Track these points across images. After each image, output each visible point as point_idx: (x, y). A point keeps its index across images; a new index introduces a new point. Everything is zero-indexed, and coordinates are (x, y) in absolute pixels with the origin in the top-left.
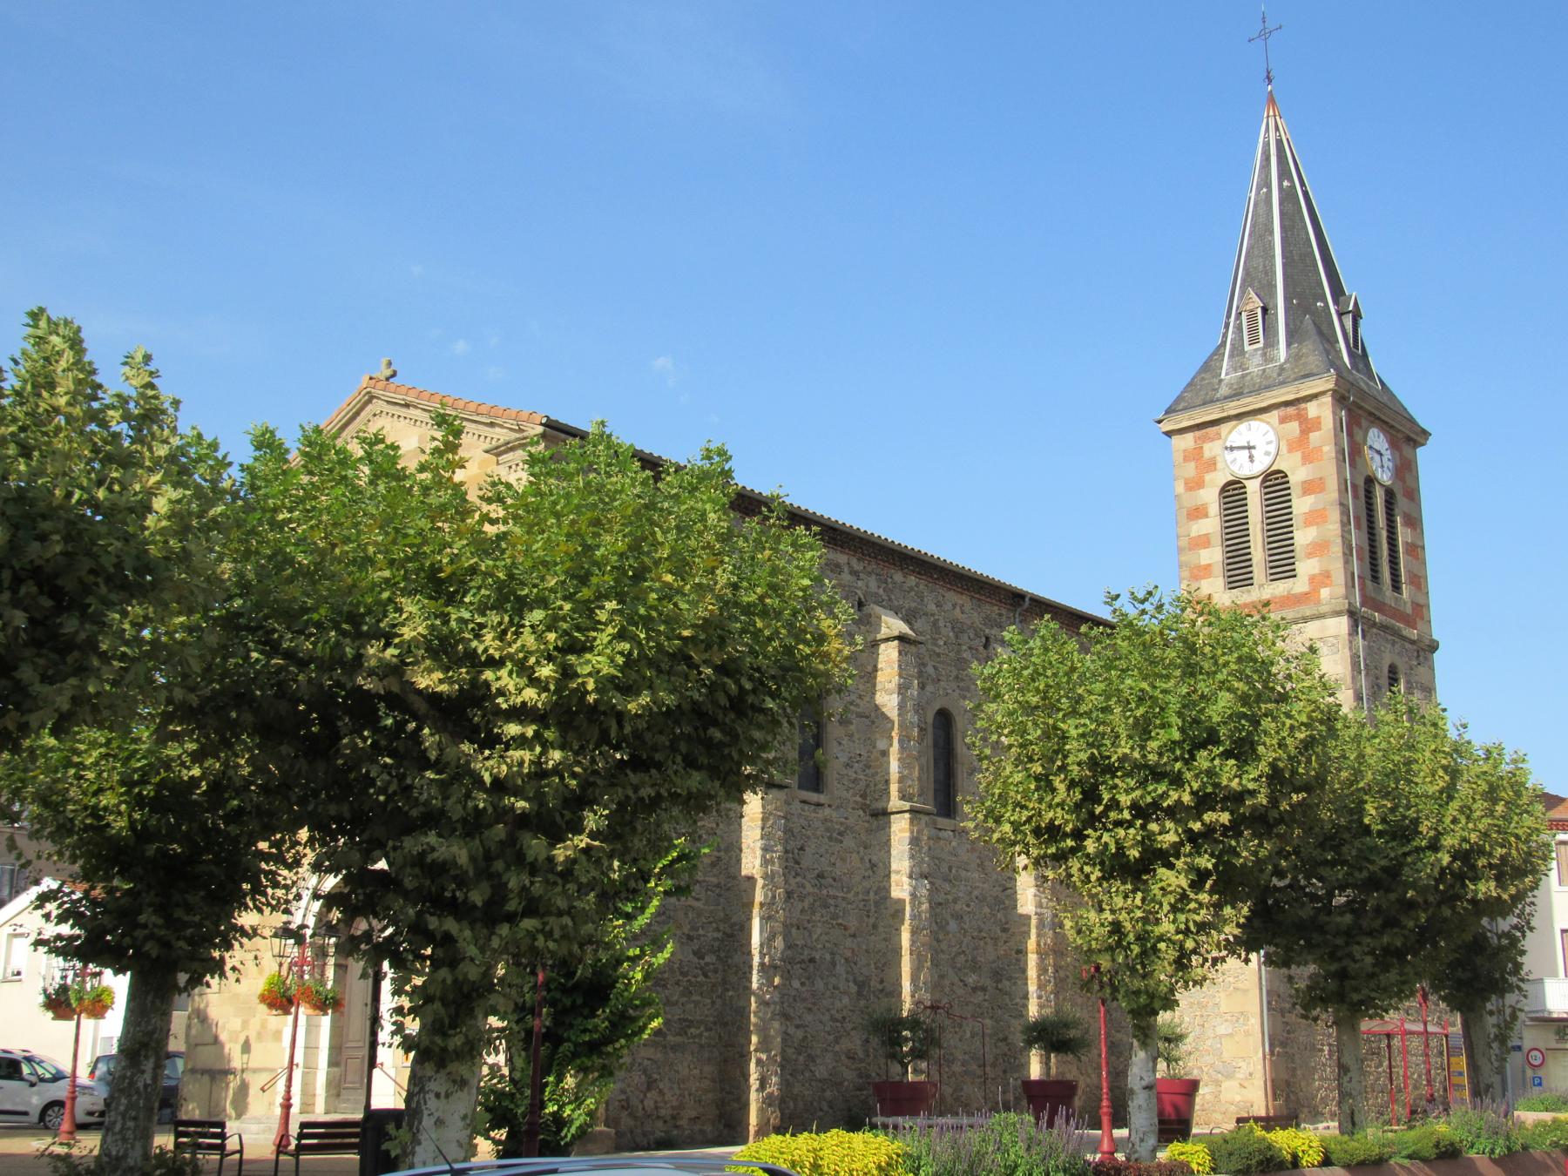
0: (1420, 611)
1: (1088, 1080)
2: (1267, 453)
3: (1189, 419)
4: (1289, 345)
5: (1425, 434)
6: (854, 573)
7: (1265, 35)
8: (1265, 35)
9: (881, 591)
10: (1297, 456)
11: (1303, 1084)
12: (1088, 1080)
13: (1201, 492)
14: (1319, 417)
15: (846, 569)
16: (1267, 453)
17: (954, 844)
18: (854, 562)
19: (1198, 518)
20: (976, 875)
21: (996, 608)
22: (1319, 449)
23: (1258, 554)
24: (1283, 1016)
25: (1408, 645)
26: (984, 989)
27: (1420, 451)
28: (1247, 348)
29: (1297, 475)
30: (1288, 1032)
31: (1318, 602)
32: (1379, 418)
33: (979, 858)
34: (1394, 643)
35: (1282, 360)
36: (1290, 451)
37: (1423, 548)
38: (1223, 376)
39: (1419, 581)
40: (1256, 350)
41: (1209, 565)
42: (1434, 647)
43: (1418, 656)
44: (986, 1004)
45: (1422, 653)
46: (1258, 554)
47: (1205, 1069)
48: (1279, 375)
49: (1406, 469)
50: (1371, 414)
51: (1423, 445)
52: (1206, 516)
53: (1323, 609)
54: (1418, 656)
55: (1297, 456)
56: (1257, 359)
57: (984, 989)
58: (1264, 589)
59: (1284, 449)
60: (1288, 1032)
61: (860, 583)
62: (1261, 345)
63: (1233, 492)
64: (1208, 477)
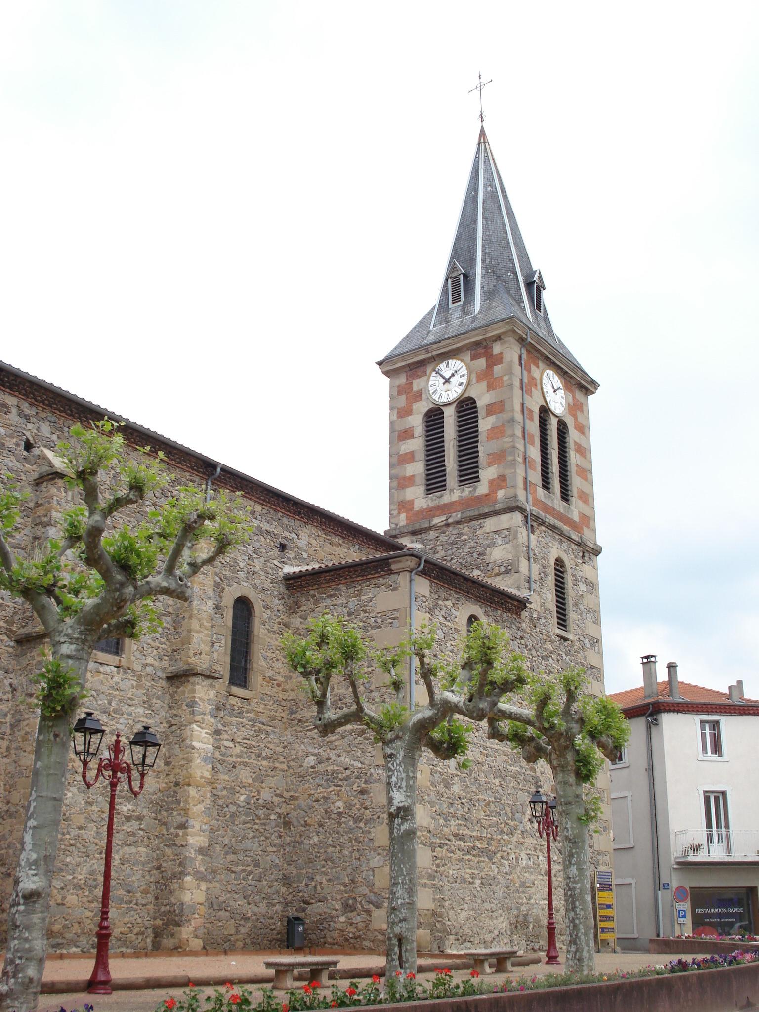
0: (588, 520)
1: (256, 909)
2: (461, 384)
3: (403, 361)
4: (483, 301)
5: (595, 384)
6: (21, 414)
7: (480, 87)
8: (480, 87)
9: (54, 437)
10: (484, 384)
11: (451, 913)
12: (256, 909)
13: (410, 418)
14: (501, 353)
15: (14, 411)
16: (461, 384)
17: (116, 679)
18: (25, 406)
19: (406, 439)
20: (141, 710)
21: (187, 474)
22: (501, 378)
23: (559, 584)
24: (433, 851)
25: (573, 546)
26: (140, 818)
27: (590, 398)
28: (451, 306)
29: (483, 400)
30: (438, 866)
31: (495, 501)
32: (554, 363)
33: (146, 694)
34: (561, 542)
35: (476, 312)
36: (477, 382)
37: (591, 472)
38: (431, 328)
39: (587, 498)
40: (457, 307)
41: (413, 476)
42: (597, 552)
43: (583, 556)
44: (141, 832)
45: (586, 555)
46: (559, 584)
47: (359, 899)
48: (472, 322)
49: (576, 408)
50: (547, 358)
51: (593, 393)
52: (412, 437)
53: (498, 506)
54: (583, 556)
55: (484, 384)
56: (458, 314)
57: (140, 818)
58: (454, 493)
59: (474, 381)
60: (438, 866)
61: (30, 426)
62: (461, 303)
63: (434, 417)
64: (415, 406)
